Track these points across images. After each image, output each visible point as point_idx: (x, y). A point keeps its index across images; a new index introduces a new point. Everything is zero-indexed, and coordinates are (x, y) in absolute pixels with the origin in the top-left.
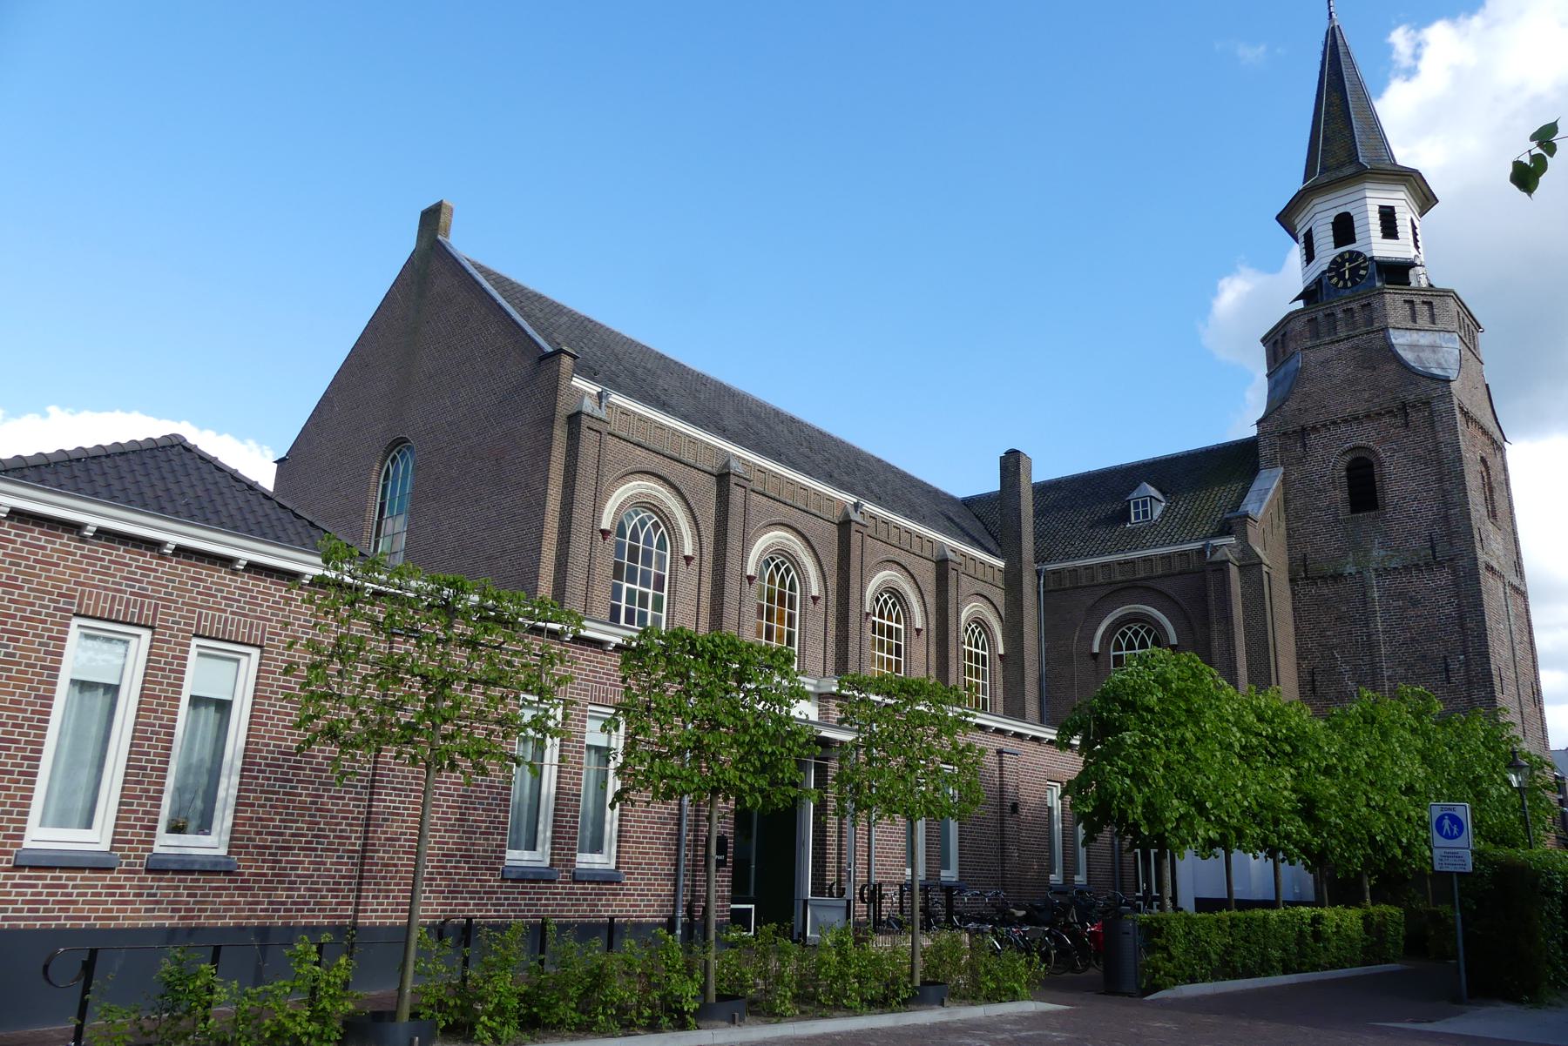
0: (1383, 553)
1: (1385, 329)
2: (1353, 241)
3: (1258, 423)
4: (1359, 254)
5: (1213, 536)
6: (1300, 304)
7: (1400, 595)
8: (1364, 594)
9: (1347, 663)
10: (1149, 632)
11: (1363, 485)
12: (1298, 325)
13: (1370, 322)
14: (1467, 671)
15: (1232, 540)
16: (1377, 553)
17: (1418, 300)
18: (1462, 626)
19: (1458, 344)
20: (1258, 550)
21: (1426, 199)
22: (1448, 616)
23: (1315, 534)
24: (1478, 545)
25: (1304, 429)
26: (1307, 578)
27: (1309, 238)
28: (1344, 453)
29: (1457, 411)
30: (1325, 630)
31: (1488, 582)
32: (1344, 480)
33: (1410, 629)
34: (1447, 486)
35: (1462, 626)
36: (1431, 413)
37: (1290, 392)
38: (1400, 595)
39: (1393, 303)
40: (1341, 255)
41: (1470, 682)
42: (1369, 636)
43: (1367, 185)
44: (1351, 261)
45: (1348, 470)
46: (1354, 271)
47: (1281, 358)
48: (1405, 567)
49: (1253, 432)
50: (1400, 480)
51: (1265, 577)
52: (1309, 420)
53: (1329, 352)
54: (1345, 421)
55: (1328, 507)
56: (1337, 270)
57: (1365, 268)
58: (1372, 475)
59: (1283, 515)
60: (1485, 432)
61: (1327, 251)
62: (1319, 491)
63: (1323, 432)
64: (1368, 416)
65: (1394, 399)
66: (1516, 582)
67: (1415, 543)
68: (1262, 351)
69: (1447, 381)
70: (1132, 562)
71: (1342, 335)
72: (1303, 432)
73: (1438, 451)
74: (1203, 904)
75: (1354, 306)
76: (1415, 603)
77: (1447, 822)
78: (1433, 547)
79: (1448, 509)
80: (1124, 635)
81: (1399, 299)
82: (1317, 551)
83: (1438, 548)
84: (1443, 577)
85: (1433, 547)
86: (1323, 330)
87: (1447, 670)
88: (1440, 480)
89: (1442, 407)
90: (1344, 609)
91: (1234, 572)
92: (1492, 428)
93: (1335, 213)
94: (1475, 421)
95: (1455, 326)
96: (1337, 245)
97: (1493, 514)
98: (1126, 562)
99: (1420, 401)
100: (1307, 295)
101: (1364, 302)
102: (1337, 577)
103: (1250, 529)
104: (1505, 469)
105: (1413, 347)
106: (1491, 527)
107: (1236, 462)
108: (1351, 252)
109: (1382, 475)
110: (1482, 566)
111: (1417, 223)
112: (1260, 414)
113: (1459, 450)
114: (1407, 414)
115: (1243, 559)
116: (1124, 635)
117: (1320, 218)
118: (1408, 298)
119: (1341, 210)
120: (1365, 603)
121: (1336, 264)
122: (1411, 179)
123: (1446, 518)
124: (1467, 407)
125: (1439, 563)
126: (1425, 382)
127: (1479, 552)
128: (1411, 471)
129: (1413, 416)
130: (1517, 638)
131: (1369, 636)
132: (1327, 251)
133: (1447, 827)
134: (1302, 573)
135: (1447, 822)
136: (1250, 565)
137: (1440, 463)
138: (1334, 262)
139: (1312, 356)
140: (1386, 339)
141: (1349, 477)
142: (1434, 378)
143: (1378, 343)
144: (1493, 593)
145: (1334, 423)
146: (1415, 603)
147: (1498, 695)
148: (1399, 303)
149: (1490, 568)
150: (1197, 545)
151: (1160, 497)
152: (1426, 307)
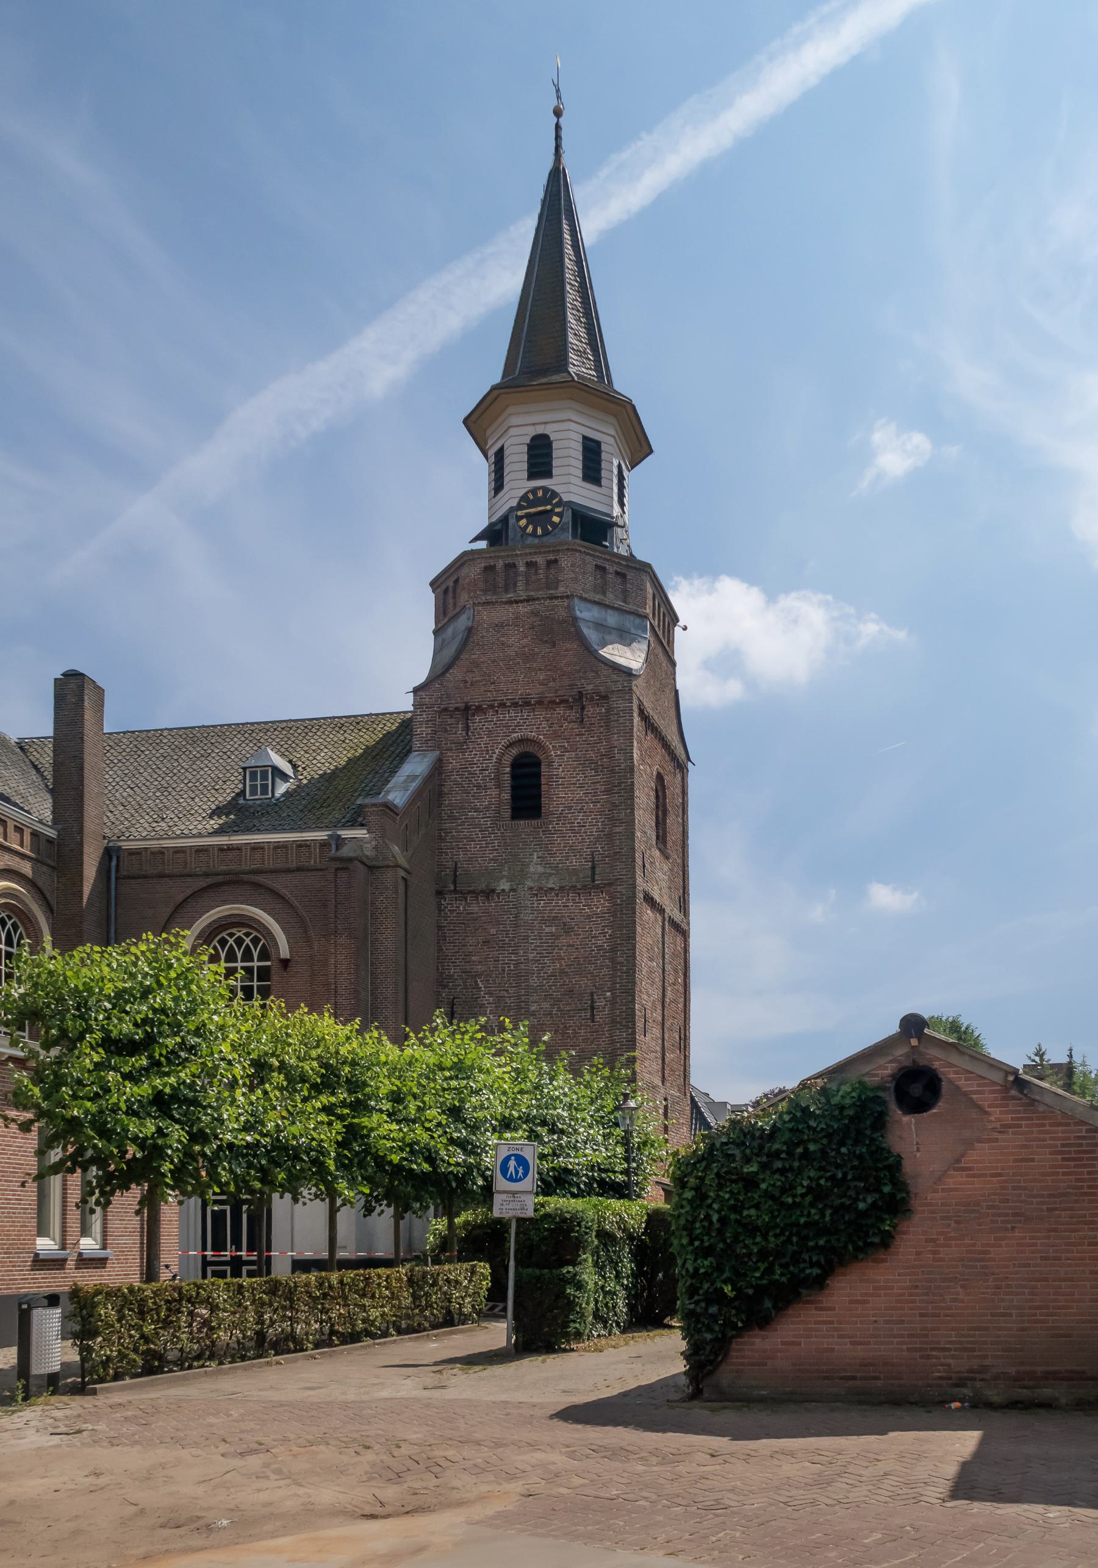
0: (540, 869)
2: (548, 474)
3: (416, 690)
4: (555, 494)
5: (344, 826)
6: (482, 545)
9: (490, 993)
10: (256, 941)
12: (473, 572)
14: (612, 1009)
17: (611, 569)
21: (639, 448)
24: (639, 872)
25: (467, 708)
26: (455, 891)
27: (500, 455)
28: (511, 745)
30: (470, 954)
33: (560, 958)
35: (613, 960)
36: (608, 711)
37: (456, 658)
40: (534, 491)
41: (614, 1021)
45: (514, 765)
47: (451, 614)
49: (405, 703)
50: (566, 786)
52: (475, 697)
53: (504, 613)
54: (515, 705)
55: (487, 808)
58: (538, 775)
60: (666, 745)
62: (479, 787)
66: (678, 917)
67: (574, 862)
68: (429, 599)
70: (238, 848)
71: (523, 595)
72: (467, 711)
74: (301, 1266)
75: (540, 560)
76: (568, 930)
77: (512, 1163)
80: (222, 942)
82: (470, 860)
83: (598, 871)
84: (600, 903)
87: (592, 1008)
89: (622, 705)
90: (493, 931)
92: (675, 742)
93: (532, 431)
96: (532, 476)
98: (230, 848)
100: (495, 534)
101: (551, 557)
102: (489, 893)
106: (657, 853)
108: (545, 490)
109: (551, 777)
111: (626, 473)
112: (421, 677)
116: (222, 942)
119: (540, 430)
121: (525, 500)
122: (625, 416)
123: (610, 836)
125: (597, 887)
127: (639, 880)
128: (580, 777)
129: (590, 710)
130: (670, 979)
131: (517, 965)
132: (518, 483)
133: (512, 1169)
135: (512, 1163)
139: (487, 616)
140: (570, 609)
141: (514, 777)
143: (562, 613)
146: (568, 930)
147: (639, 1037)
148: (590, 568)
149: (649, 899)
150: (321, 835)
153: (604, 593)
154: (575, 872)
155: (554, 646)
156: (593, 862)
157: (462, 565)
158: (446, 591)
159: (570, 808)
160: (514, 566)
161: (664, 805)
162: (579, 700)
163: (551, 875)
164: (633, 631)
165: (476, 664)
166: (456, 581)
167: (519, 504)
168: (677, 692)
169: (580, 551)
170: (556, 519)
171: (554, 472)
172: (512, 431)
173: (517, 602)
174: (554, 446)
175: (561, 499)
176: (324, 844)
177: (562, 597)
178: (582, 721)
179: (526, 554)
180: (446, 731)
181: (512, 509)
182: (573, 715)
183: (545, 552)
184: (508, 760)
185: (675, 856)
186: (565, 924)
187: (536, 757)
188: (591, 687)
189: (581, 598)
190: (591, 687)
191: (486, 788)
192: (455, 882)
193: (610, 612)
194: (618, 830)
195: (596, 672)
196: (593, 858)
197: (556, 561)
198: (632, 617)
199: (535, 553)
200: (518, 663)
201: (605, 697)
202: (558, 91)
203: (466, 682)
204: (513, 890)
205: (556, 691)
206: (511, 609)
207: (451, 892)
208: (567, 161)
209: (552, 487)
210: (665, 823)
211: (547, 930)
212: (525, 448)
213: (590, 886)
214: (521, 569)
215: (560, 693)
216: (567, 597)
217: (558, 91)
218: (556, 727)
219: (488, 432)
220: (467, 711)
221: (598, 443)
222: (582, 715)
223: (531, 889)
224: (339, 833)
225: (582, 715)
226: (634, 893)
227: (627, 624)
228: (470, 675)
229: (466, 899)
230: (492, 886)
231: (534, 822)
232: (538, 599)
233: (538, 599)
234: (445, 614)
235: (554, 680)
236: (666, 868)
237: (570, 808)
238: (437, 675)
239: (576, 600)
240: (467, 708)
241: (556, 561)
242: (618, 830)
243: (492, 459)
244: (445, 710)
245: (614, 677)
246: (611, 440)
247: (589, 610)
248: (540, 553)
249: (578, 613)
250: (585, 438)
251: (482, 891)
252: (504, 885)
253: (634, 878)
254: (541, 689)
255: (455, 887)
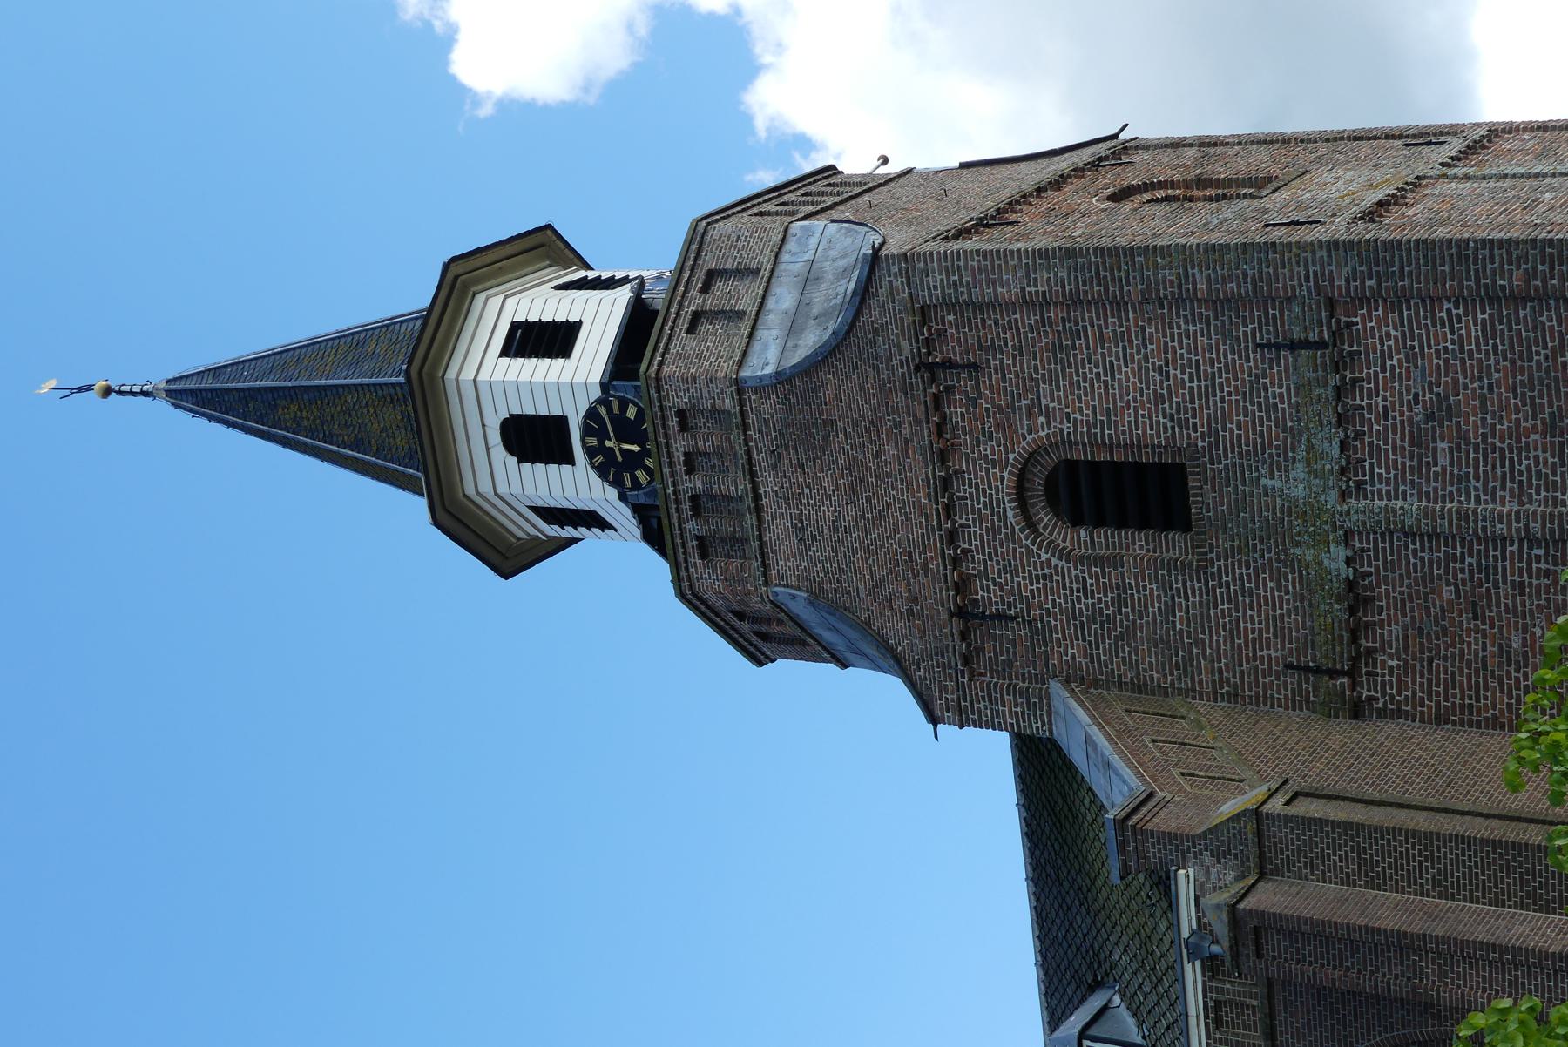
0: (1299, 471)
1: (740, 387)
3: (934, 720)
4: (591, 414)
7: (1419, 441)
8: (1411, 534)
11: (1122, 492)
12: (710, 581)
13: (717, 414)
15: (1186, 881)
16: (1297, 484)
17: (695, 302)
18: (1518, 299)
19: (818, 224)
20: (1229, 808)
21: (543, 248)
22: (1489, 331)
23: (1234, 630)
25: (961, 613)
26: (1352, 673)
28: (1031, 524)
29: (956, 246)
30: (1505, 651)
31: (1415, 221)
32: (1100, 535)
33: (1516, 433)
34: (1134, 291)
35: (1518, 299)
36: (951, 307)
37: (865, 627)
38: (1419, 441)
39: (688, 360)
40: (590, 453)
42: (1533, 542)
43: (451, 374)
44: (603, 435)
45: (1076, 521)
46: (628, 431)
47: (789, 629)
48: (1341, 421)
50: (1114, 401)
51: (1305, 808)
52: (937, 595)
53: (780, 528)
54: (949, 510)
55: (1166, 586)
56: (621, 468)
57: (624, 404)
58: (1094, 466)
59: (1175, 702)
61: (577, 484)
62: (1120, 602)
63: (972, 567)
64: (943, 457)
65: (907, 388)
66: (1455, 145)
67: (1280, 389)
68: (786, 670)
69: (875, 259)
71: (744, 485)
72: (967, 615)
73: (1043, 303)
75: (680, 446)
76: (1444, 411)
78: (1294, 346)
79: (1194, 298)
81: (684, 343)
82: (1280, 634)
83: (1297, 333)
84: (1377, 330)
85: (1294, 346)
86: (725, 528)
88: (1119, 305)
89: (936, 277)
90: (1448, 592)
91: (1270, 898)
93: (499, 452)
94: (1011, 206)
95: (775, 225)
96: (564, 456)
97: (1260, 184)
99: (916, 329)
101: (673, 423)
102: (1356, 595)
103: (1165, 821)
104: (1177, 144)
105: (793, 329)
106: (1284, 194)
107: (1046, 779)
108: (586, 431)
110: (1368, 232)
113: (1044, 253)
114: (948, 364)
115: (1242, 859)
117: (516, 486)
118: (683, 323)
119: (495, 437)
120: (1433, 535)
121: (609, 468)
122: (463, 278)
123: (1218, 304)
124: (962, 219)
125: (1337, 334)
126: (873, 313)
127: (1321, 234)
129: (951, 349)
131: (1533, 542)
132: (577, 484)
134: (1340, 680)
136: (1258, 844)
137: (1075, 300)
138: (602, 471)
139: (786, 560)
140: (762, 386)
141: (1099, 522)
142: (865, 291)
143: (771, 407)
144: (1462, 209)
145: (952, 538)
146: (1444, 411)
148: (691, 344)
150: (1193, 975)
151: (1095, 1003)
152: (719, 287)
153: (740, 315)
154: (1303, 388)
155: (833, 423)
156: (1278, 346)
157: (704, 602)
158: (765, 637)
159: (1159, 398)
160: (695, 499)
161: (1187, 184)
162: (932, 369)
163: (1310, 448)
164: (808, 256)
165: (876, 587)
166: (741, 616)
167: (612, 484)
168: (965, 166)
169: (661, 364)
170: (631, 413)
171: (556, 412)
172: (502, 489)
173: (757, 497)
174: (517, 411)
175: (599, 401)
176: (1212, 967)
177: (742, 403)
178: (975, 366)
179: (673, 474)
180: (1009, 663)
181: (623, 497)
182: (964, 383)
183: (666, 436)
184: (1063, 535)
185: (1305, 158)
186: (1430, 417)
187: (1055, 469)
188: (905, 344)
189: (740, 364)
190: (905, 344)
191: (1124, 587)
192: (1333, 673)
193: (771, 303)
194: (1202, 285)
195: (876, 332)
196: (1269, 345)
197: (681, 414)
198: (784, 257)
199: (669, 455)
200: (869, 500)
201: (924, 311)
202: (80, 390)
203: (910, 612)
204: (1347, 537)
205: (918, 422)
206: (771, 508)
207: (1354, 685)
208: (158, 376)
209: (582, 413)
210: (1228, 183)
211: (1443, 460)
212: (527, 466)
213: (1334, 350)
214: (699, 484)
215: (921, 415)
216: (740, 392)
217: (80, 390)
218: (990, 425)
219: (521, 535)
220: (967, 615)
221: (515, 326)
222: (963, 367)
223: (1344, 495)
224: (1185, 934)
225: (963, 367)
226: (1349, 245)
227: (796, 267)
228: (897, 603)
229: (1370, 652)
230: (1338, 587)
231: (1192, 482)
232: (748, 453)
233: (748, 453)
234: (804, 645)
235: (897, 425)
236: (1327, 177)
237: (1159, 398)
238: (900, 666)
239: (746, 373)
240: (961, 613)
241: (681, 414)
242: (1202, 285)
243: (569, 532)
244: (967, 660)
245: (883, 292)
246: (511, 302)
247: (766, 347)
248: (668, 445)
249: (769, 370)
250: (505, 352)
251: (1352, 610)
252: (1336, 559)
253: (1312, 247)
254: (916, 454)
255: (1342, 673)
